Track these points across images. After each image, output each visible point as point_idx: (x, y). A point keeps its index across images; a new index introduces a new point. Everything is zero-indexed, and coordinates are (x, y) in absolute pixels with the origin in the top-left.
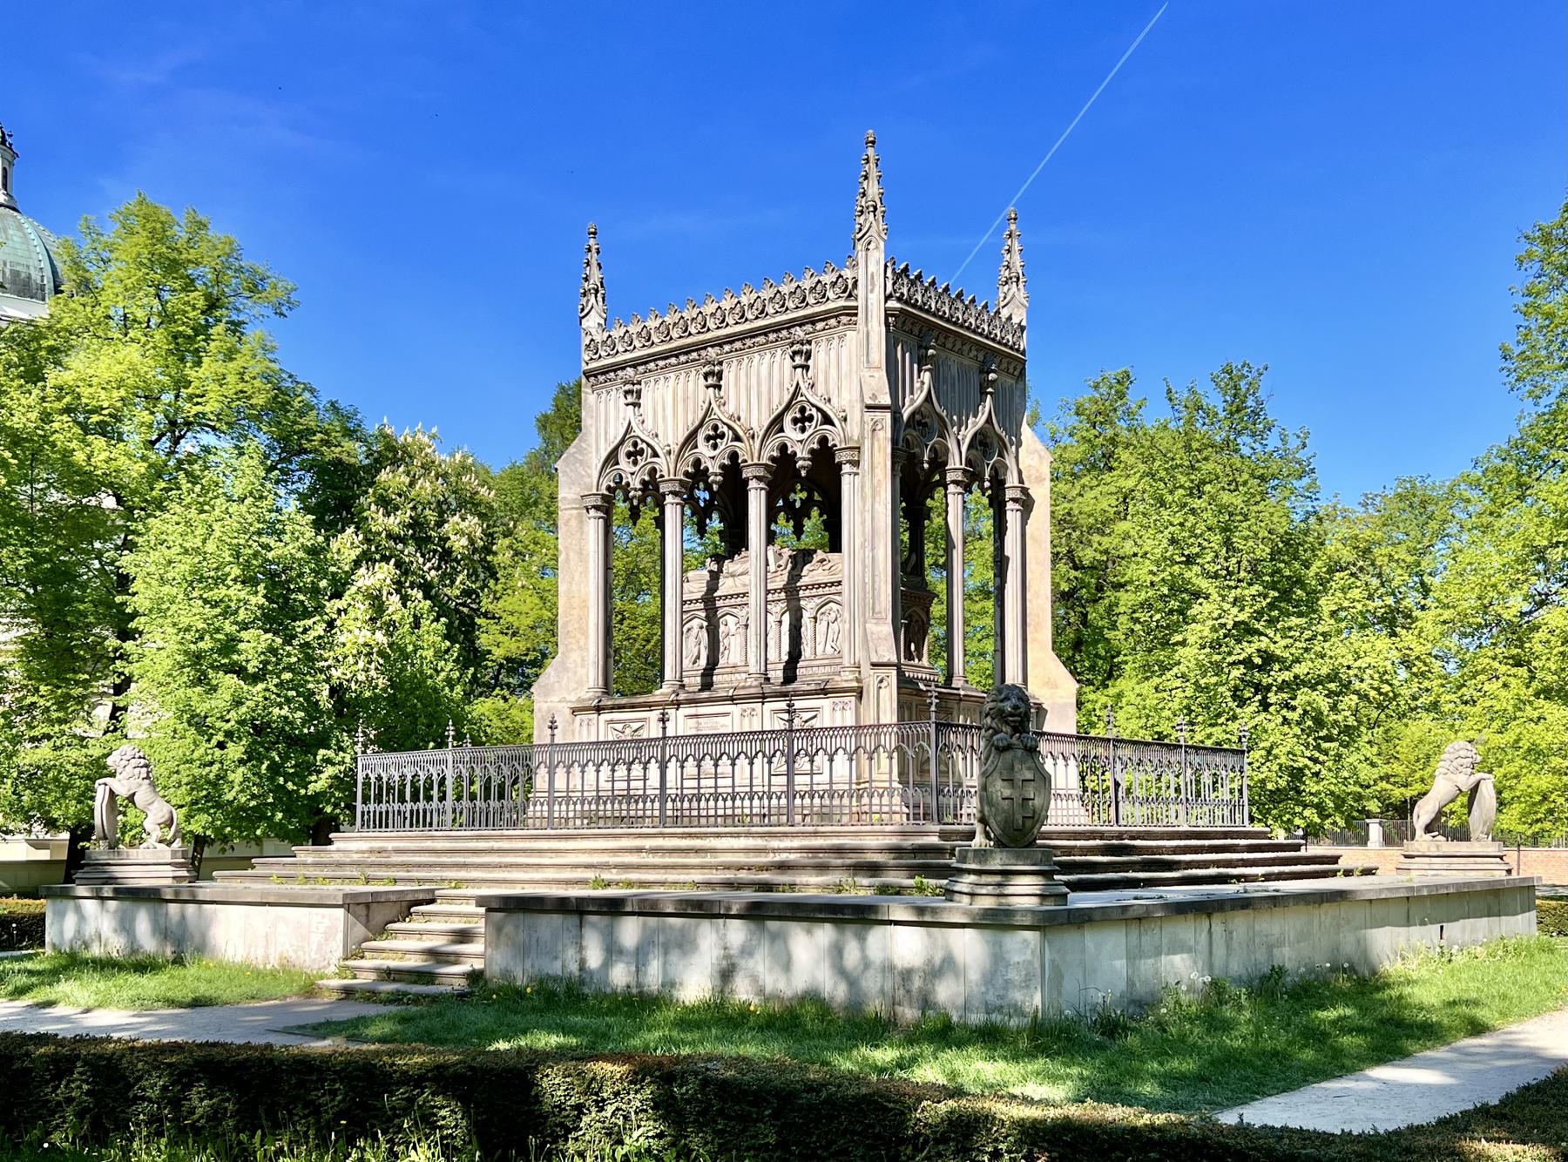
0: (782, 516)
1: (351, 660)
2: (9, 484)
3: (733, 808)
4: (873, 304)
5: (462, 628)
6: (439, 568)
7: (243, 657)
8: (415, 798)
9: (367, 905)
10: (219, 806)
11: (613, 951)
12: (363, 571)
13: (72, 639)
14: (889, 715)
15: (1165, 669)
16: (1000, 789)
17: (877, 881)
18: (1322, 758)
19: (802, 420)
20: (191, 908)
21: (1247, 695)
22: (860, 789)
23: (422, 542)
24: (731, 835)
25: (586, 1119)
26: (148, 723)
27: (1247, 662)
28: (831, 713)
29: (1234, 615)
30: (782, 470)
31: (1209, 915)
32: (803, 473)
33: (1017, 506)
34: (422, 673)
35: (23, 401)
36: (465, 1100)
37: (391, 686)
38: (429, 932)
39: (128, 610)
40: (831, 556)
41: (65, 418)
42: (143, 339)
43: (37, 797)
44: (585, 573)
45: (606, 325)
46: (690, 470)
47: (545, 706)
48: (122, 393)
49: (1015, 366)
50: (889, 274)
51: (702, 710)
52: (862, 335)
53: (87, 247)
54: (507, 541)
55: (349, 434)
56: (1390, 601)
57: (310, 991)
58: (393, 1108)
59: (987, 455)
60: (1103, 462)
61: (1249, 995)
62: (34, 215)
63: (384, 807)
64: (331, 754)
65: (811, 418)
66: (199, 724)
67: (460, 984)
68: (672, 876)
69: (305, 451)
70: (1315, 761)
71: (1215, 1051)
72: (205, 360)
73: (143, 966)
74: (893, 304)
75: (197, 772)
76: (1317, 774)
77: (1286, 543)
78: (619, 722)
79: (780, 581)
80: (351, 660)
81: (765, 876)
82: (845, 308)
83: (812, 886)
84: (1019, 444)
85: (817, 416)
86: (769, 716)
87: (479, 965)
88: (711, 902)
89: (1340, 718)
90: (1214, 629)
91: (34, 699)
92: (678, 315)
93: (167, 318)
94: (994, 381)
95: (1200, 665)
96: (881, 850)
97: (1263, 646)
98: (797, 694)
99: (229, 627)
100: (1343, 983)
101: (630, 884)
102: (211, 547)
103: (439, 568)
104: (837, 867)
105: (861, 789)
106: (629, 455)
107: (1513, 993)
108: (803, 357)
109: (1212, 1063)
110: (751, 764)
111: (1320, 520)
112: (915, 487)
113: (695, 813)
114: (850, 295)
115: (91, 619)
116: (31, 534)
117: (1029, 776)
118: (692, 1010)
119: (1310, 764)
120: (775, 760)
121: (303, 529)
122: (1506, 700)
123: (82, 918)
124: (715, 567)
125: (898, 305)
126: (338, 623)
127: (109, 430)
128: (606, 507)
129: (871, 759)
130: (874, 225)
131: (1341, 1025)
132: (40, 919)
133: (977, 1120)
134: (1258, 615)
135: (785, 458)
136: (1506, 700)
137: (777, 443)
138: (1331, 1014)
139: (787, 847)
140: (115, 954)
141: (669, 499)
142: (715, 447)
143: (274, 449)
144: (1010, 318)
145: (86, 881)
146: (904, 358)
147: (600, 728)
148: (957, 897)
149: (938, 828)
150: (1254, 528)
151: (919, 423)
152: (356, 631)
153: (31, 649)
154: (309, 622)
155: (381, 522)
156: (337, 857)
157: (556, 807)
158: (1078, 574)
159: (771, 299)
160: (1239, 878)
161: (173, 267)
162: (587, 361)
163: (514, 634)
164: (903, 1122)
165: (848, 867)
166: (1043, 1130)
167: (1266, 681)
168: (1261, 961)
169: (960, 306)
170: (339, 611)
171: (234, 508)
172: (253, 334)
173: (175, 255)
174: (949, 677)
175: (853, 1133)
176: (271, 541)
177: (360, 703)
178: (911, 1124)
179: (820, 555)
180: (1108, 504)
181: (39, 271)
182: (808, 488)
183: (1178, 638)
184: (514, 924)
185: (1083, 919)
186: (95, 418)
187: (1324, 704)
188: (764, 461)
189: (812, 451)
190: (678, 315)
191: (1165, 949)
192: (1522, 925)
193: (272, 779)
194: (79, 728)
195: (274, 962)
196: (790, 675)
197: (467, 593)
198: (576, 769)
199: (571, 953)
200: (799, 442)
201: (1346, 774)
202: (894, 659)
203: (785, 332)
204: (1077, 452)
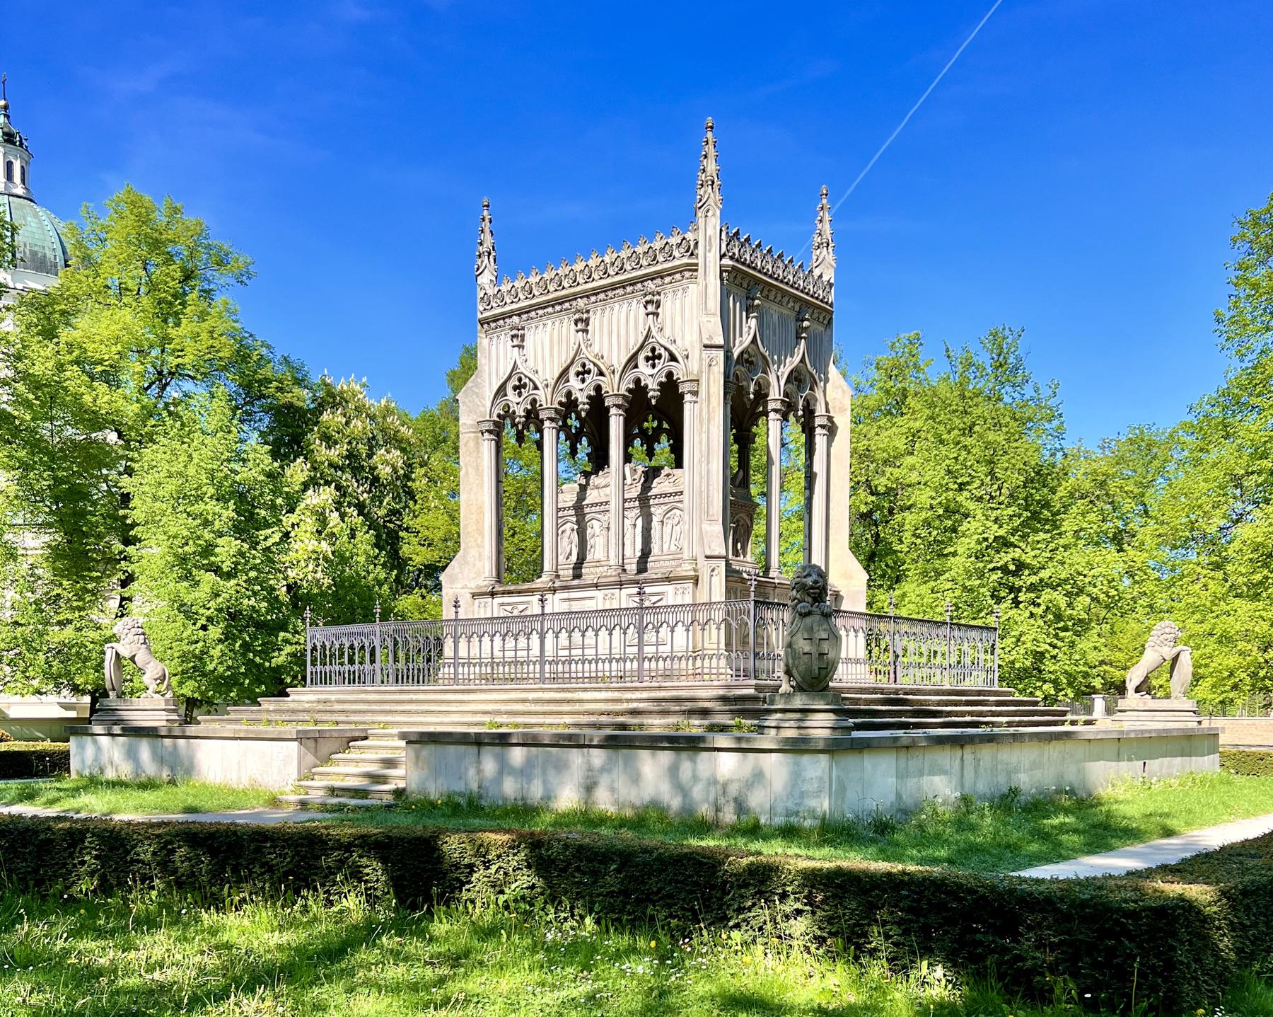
0: (637, 442)
1: (303, 564)
2: (33, 419)
4: (711, 262)
5: (388, 540)
6: (370, 491)
7: (219, 559)
8: (351, 661)
9: (315, 739)
10: (204, 675)
11: (504, 767)
12: (310, 492)
13: (87, 544)
14: (719, 594)
15: (939, 574)
16: (803, 646)
17: (706, 722)
18: (1060, 644)
19: (653, 358)
20: (181, 742)
21: (1003, 594)
22: (696, 654)
23: (356, 470)
24: (595, 689)
25: (476, 875)
26: (147, 611)
27: (1004, 569)
28: (672, 595)
29: (995, 531)
30: (637, 399)
31: (962, 746)
32: (653, 402)
33: (824, 431)
34: (358, 575)
35: (42, 354)
36: (384, 860)
37: (335, 585)
38: (363, 761)
39: (128, 521)
40: (675, 471)
41: (75, 368)
42: (134, 304)
43: (64, 668)
44: (481, 484)
45: (498, 280)
46: (564, 400)
48: (119, 347)
49: (824, 315)
50: (724, 234)
51: (573, 595)
52: (702, 287)
53: (88, 229)
54: (423, 471)
55: (299, 382)
56: (1120, 524)
57: (275, 802)
58: (329, 867)
59: (800, 388)
60: (897, 405)
61: (991, 807)
62: (43, 205)
63: (328, 668)
64: (289, 636)
65: (659, 357)
66: (187, 612)
67: (388, 799)
68: (549, 720)
69: (264, 397)
70: (1055, 647)
71: (962, 845)
72: (184, 321)
73: (148, 785)
74: (727, 261)
75: (185, 648)
76: (1054, 657)
77: (1038, 473)
78: (509, 604)
79: (635, 491)
80: (303, 564)
81: (621, 719)
82: (688, 265)
83: (657, 725)
84: (827, 381)
85: (665, 355)
86: (625, 598)
87: (402, 785)
88: (578, 735)
89: (1075, 613)
90: (978, 542)
91: (59, 591)
92: (554, 272)
93: (153, 287)
94: (806, 328)
95: (966, 571)
96: (710, 700)
97: (1017, 556)
98: (646, 581)
99: (208, 535)
100: (1065, 801)
101: (517, 725)
102: (191, 471)
103: (370, 491)
104: (675, 712)
105: (695, 653)
106: (515, 388)
107: (1197, 809)
108: (653, 305)
109: (959, 851)
110: (611, 634)
111: (1065, 455)
112: (743, 416)
113: (567, 675)
114: (692, 254)
115: (101, 529)
116: (53, 460)
117: (824, 636)
118: (564, 815)
119: (1050, 649)
121: (260, 458)
122: (1205, 599)
123: (99, 749)
124: (583, 481)
125: (731, 263)
126: (292, 534)
127: (111, 378)
128: (497, 430)
129: (703, 630)
130: (712, 197)
131: (1062, 829)
132: (66, 755)
133: (771, 870)
134: (1014, 531)
135: (639, 390)
136: (1205, 599)
137: (632, 377)
138: (1055, 821)
139: (637, 698)
140: (123, 778)
141: (547, 424)
142: (583, 381)
143: (240, 395)
144: (821, 276)
145: (101, 722)
146: (735, 307)
147: (494, 608)
148: (766, 731)
149: (754, 682)
150: (1013, 461)
151: (747, 361)
152: (307, 541)
153: (56, 553)
154: (270, 531)
155: (323, 453)
156: (292, 705)
157: (460, 670)
158: (873, 498)
159: (629, 258)
160: (987, 723)
161: (156, 245)
162: (482, 312)
163: (429, 545)
164: (714, 873)
165: (683, 712)
166: (821, 876)
167: (1018, 583)
168: (1003, 785)
169: (781, 265)
170: (293, 525)
171: (208, 440)
172: (220, 300)
173: (156, 235)
174: (767, 569)
175: (677, 882)
176: (236, 467)
177: (309, 598)
178: (720, 874)
179: (666, 470)
180: (901, 444)
181: (52, 251)
182: (656, 416)
183: (952, 550)
184: (428, 751)
185: (862, 746)
186: (99, 368)
187: (1062, 601)
188: (622, 391)
189: (661, 384)
190: (554, 272)
191: (926, 772)
192: (1208, 764)
193: (244, 655)
194: (94, 615)
195: (245, 782)
196: (642, 566)
197: (393, 512)
198: (475, 639)
199: (472, 772)
200: (651, 377)
201: (1077, 657)
202: (723, 553)
203: (639, 285)
204: (874, 398)
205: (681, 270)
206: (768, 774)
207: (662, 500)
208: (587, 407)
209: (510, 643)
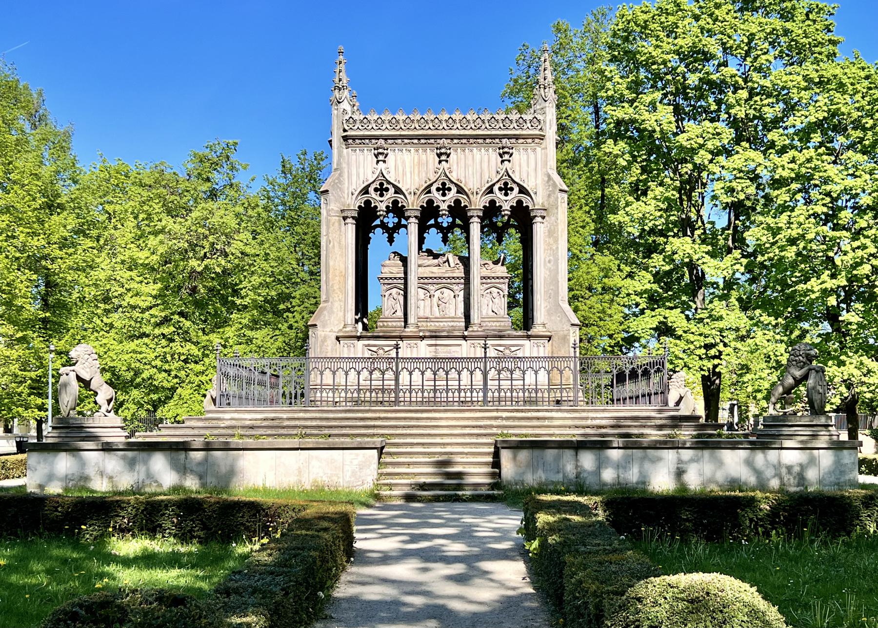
3: (423, 397)
30: (429, 212)
47: (323, 333)
78: (500, 345)
189: (512, 207)
200: (506, 202)
205: (533, 137)
206: (38, 482)
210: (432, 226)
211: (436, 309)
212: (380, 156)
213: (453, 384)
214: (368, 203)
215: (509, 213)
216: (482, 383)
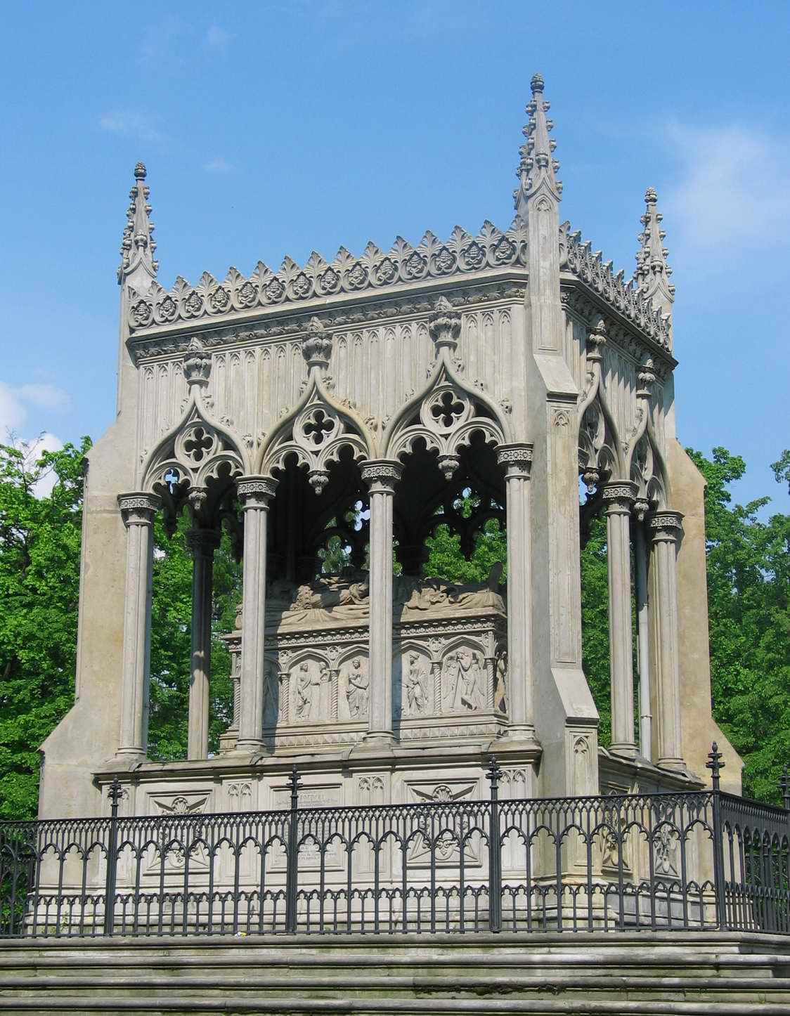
4: (545, 266)
30: (418, 467)
46: (281, 466)
74: (570, 276)
114: (518, 261)
120: (411, 844)
137: (410, 436)
189: (460, 449)
200: (448, 441)
207: (441, 630)
208: (454, 463)
209: (174, 860)
210: (441, 519)
211: (343, 704)
212: (317, 355)
213: (364, 880)
214: (419, 443)
215: (454, 463)
216: (556, 871)
